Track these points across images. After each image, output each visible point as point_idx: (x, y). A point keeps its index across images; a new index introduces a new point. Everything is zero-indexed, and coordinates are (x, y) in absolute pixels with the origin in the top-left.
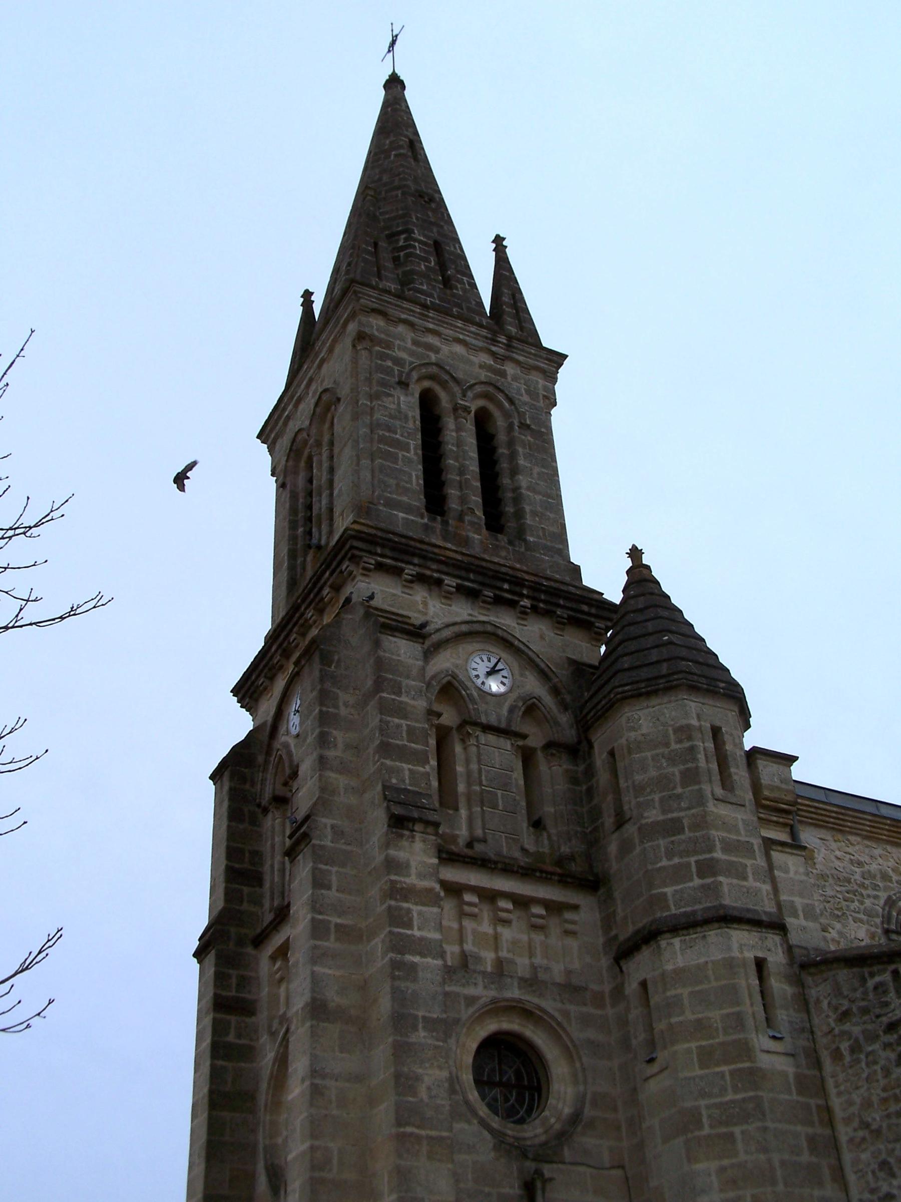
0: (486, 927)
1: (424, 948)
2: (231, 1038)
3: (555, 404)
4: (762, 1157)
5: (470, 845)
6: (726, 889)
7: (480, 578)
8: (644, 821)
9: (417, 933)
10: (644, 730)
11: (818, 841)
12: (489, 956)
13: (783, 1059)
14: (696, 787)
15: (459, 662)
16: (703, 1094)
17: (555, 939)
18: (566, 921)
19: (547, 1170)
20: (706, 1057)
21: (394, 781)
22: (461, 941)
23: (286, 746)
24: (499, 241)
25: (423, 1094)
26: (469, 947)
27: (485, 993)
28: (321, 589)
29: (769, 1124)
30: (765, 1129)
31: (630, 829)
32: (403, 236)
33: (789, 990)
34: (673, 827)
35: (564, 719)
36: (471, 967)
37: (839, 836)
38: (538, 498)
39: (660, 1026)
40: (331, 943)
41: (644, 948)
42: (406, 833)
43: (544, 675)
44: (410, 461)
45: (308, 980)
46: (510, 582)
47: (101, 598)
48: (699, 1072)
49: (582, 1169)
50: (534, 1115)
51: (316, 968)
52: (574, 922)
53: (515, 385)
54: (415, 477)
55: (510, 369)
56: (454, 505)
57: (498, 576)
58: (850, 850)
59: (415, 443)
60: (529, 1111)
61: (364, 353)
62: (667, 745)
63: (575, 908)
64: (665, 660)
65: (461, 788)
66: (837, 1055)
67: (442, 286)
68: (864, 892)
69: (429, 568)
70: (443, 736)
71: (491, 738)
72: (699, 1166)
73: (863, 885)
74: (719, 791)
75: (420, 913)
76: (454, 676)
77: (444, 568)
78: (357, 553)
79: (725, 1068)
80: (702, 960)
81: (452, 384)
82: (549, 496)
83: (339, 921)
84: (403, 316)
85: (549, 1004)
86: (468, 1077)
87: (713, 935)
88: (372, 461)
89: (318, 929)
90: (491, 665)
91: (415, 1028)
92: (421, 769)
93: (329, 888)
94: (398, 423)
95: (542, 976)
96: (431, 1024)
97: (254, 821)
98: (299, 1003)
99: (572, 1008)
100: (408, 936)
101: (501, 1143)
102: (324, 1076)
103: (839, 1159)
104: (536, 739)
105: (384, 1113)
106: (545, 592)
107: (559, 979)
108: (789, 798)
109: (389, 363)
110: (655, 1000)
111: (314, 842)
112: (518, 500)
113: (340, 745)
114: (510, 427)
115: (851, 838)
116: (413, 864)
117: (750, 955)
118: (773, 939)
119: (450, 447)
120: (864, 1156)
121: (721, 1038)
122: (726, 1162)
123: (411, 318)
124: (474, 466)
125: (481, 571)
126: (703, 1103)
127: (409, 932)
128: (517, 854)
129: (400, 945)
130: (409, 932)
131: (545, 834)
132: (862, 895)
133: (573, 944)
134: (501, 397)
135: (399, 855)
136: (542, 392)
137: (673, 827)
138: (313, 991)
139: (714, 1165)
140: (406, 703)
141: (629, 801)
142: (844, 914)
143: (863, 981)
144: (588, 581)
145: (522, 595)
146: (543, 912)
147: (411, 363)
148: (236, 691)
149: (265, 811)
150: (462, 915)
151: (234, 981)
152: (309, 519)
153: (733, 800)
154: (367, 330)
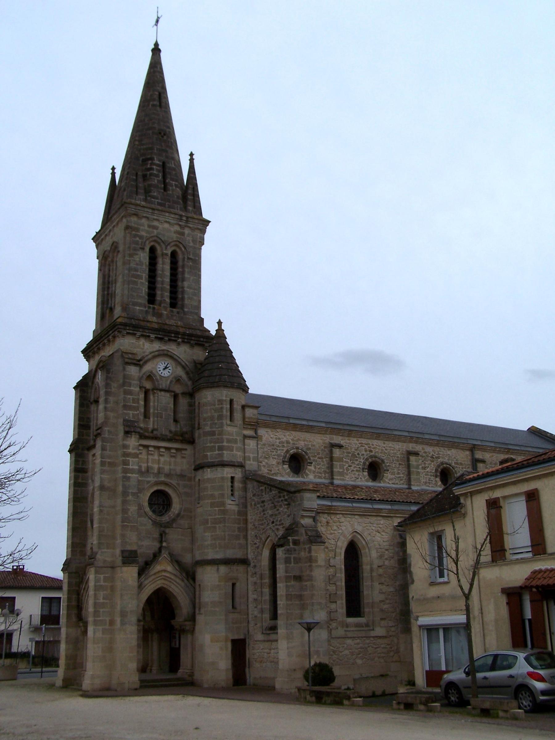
0: (156, 457)
1: (132, 471)
2: (80, 481)
3: (203, 244)
4: (223, 533)
5: (152, 432)
6: (225, 455)
7: (163, 333)
8: (204, 430)
9: (131, 467)
10: (209, 399)
11: (265, 432)
12: (156, 466)
13: (234, 506)
14: (221, 421)
15: (154, 366)
16: (210, 515)
17: (179, 459)
18: (183, 454)
19: (167, 530)
20: (212, 505)
21: (127, 418)
22: (148, 462)
23: (98, 383)
24: (191, 155)
25: (130, 514)
26: (150, 464)
27: (153, 479)
28: (109, 336)
29: (227, 525)
30: (225, 526)
31: (201, 431)
32: (150, 162)
33: (241, 485)
34: (213, 433)
35: (190, 383)
36: (150, 471)
37: (274, 430)
38: (191, 291)
39: (202, 494)
40: (106, 468)
41: (201, 470)
42: (130, 435)
43: (183, 367)
44: (142, 283)
45: (99, 479)
46: (175, 334)
47: (53, 672)
48: (210, 509)
49: (179, 529)
50: (167, 512)
51: (102, 476)
52: (185, 454)
53: (188, 238)
54: (144, 289)
55: (187, 231)
56: (158, 298)
57: (170, 332)
58: (276, 434)
59: (145, 276)
60: (166, 512)
61: (128, 235)
62: (215, 405)
63: (186, 449)
64: (218, 375)
65: (152, 411)
66: (251, 504)
67: (163, 191)
68: (278, 448)
69: (146, 332)
70: (146, 392)
71: (163, 393)
72: (206, 534)
73: (278, 446)
74: (229, 422)
75: (132, 461)
76: (151, 372)
77: (150, 331)
78: (120, 330)
79: (217, 509)
80: (215, 477)
81: (162, 244)
82: (195, 289)
83: (109, 461)
84: (145, 215)
85: (174, 482)
86: (146, 504)
87: (219, 469)
88: (129, 285)
89: (103, 463)
90: (165, 365)
91: (128, 496)
92: (136, 412)
93: (106, 450)
94: (139, 267)
95: (172, 472)
96: (133, 494)
97: (88, 407)
98: (97, 484)
99: (181, 482)
100: (128, 468)
101: (155, 523)
102: (103, 507)
103: (247, 533)
104: (178, 389)
105: (119, 517)
106: (188, 336)
107: (178, 472)
108: (255, 421)
109: (138, 239)
110: (201, 486)
111: (102, 436)
112: (183, 292)
113: (112, 402)
114: (184, 258)
115: (277, 430)
116: (131, 445)
117: (229, 476)
118: (239, 470)
119: (159, 272)
120: (253, 533)
121: (217, 500)
122: (213, 534)
123: (148, 215)
124: (167, 280)
125: (164, 331)
126: (209, 517)
127: (128, 467)
128: (168, 433)
129: (125, 471)
130: (128, 467)
131: (179, 424)
132: (277, 450)
133: (185, 461)
134: (181, 246)
135: (127, 443)
136: (199, 240)
137: (213, 433)
138: (101, 482)
139: (209, 534)
140: (133, 390)
141: (202, 421)
142: (269, 457)
143: (259, 487)
144: (206, 325)
145: (178, 338)
146: (175, 452)
147: (147, 236)
148: (83, 352)
149: (91, 403)
150: (148, 454)
151: (81, 463)
152: (109, 283)
153: (233, 425)
154: (130, 224)
